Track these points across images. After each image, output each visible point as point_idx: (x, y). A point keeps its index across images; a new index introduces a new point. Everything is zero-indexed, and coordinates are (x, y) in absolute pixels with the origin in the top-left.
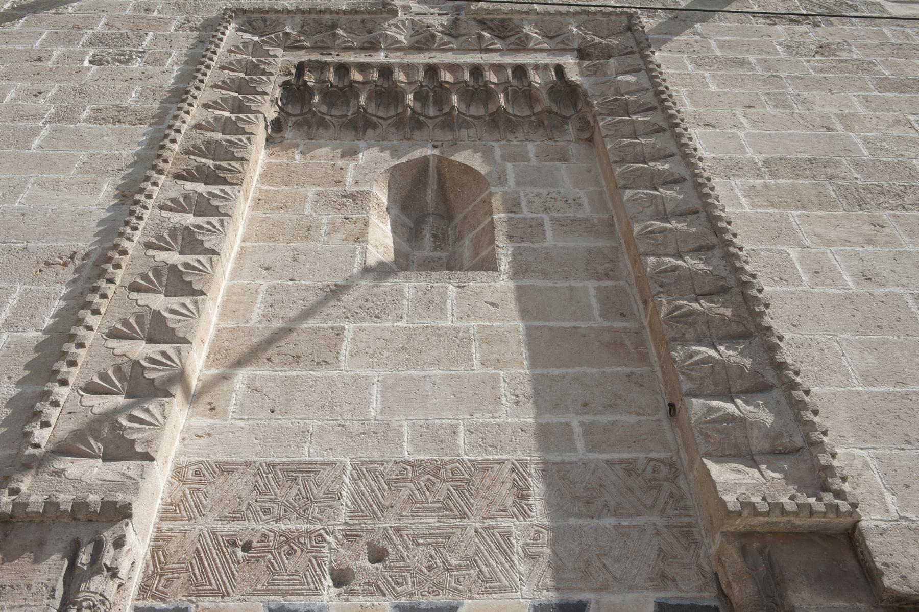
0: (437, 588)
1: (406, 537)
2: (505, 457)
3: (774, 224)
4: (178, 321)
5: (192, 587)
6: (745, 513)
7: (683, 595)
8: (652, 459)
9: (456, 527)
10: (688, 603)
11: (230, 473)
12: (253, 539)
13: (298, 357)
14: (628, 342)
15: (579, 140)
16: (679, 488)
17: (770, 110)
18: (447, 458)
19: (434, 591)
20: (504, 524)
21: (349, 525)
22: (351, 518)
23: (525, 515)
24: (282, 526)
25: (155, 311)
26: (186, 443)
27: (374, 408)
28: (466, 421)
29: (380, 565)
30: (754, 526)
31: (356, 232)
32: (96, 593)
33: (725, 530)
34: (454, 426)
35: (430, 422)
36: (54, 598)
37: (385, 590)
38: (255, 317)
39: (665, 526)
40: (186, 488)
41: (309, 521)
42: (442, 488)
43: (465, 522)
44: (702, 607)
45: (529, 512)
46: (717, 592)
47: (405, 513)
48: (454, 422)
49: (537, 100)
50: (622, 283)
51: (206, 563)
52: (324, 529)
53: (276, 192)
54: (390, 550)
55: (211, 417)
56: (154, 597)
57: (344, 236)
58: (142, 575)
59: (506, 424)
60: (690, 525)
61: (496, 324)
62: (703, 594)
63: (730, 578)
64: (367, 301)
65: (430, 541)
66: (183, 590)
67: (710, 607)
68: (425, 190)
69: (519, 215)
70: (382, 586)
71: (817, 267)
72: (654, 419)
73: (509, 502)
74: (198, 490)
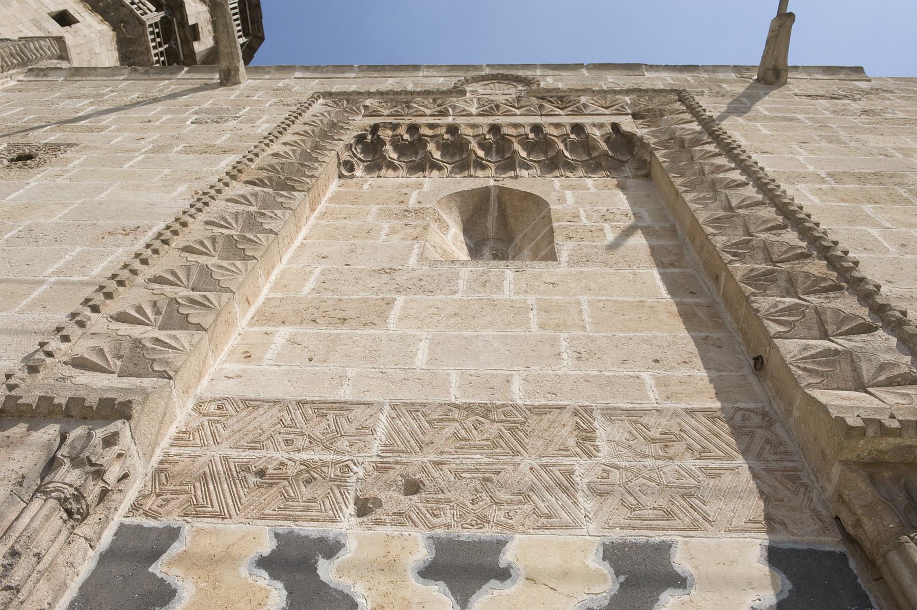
0: (483, 520)
2: (566, 403)
3: (848, 213)
4: (224, 275)
5: (191, 508)
6: (870, 432)
8: (740, 409)
9: (507, 463)
10: (804, 547)
11: (255, 408)
12: (269, 466)
14: (700, 314)
15: (636, 177)
16: (776, 435)
17: (824, 144)
18: (499, 403)
21: (382, 457)
22: (383, 451)
23: (590, 455)
24: (304, 456)
25: (202, 265)
26: (213, 382)
28: (521, 372)
29: (415, 497)
31: (415, 233)
32: (71, 486)
33: (844, 458)
34: (507, 376)
35: (480, 372)
37: (417, 520)
39: (765, 470)
40: (205, 420)
42: (492, 429)
43: (517, 459)
44: (824, 552)
45: (595, 452)
46: (840, 537)
47: (447, 449)
48: (508, 372)
51: (211, 487)
52: (352, 460)
53: (340, 209)
54: (427, 482)
55: (245, 363)
56: (146, 514)
57: (403, 236)
60: (794, 469)
61: (555, 298)
62: (822, 538)
63: (859, 512)
64: (421, 280)
66: (179, 510)
68: (486, 217)
69: (579, 224)
71: (903, 242)
72: (738, 374)
73: (571, 442)
74: (218, 421)
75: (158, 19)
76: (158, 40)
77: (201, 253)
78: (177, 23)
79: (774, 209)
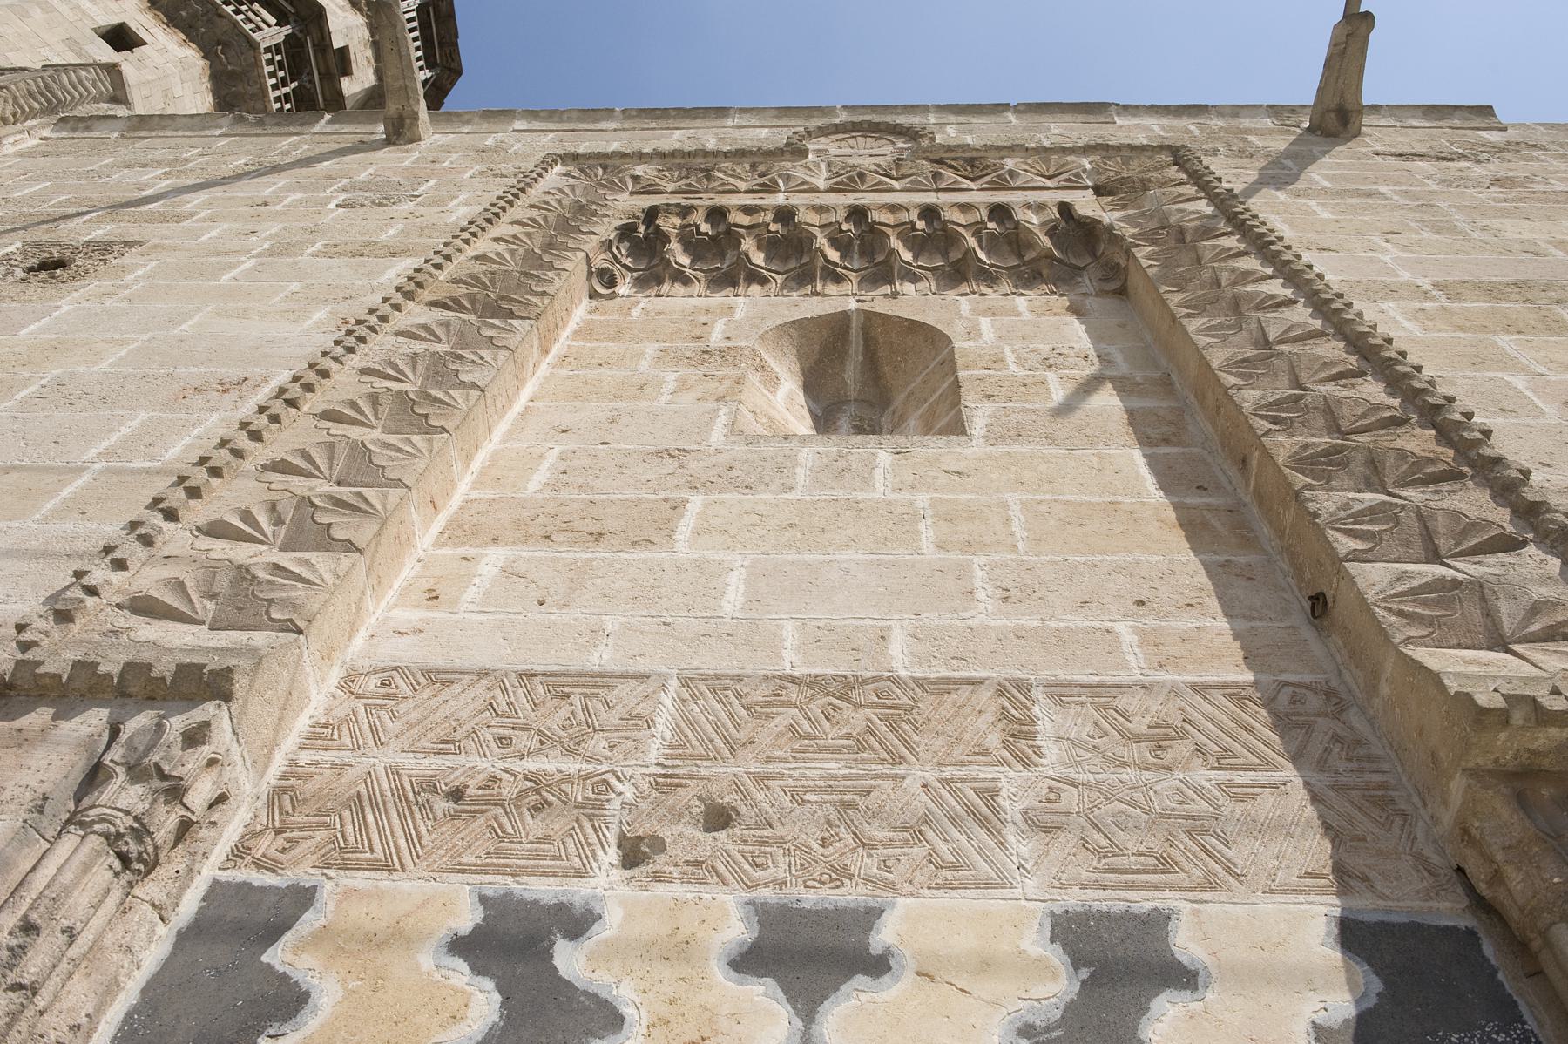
0: (841, 874)
1: (778, 790)
2: (983, 674)
5: (335, 854)
6: (1517, 718)
7: (1390, 903)
8: (1286, 684)
9: (882, 777)
10: (1404, 919)
11: (446, 684)
12: (470, 783)
13: (601, 534)
15: (1101, 293)
16: (1351, 728)
19: (832, 881)
20: (983, 776)
22: (667, 757)
24: (531, 765)
25: (355, 442)
26: (374, 641)
27: (733, 599)
28: (906, 623)
30: (1535, 753)
32: (127, 813)
33: (1471, 765)
34: (881, 629)
36: (41, 812)
38: (532, 487)
39: (1332, 787)
40: (360, 705)
41: (588, 759)
42: (856, 719)
43: (899, 770)
47: (778, 753)
48: (883, 623)
49: (1031, 245)
50: (1196, 450)
51: (370, 818)
52: (613, 772)
54: (743, 809)
56: (257, 865)
58: (241, 830)
59: (985, 627)
60: (1383, 786)
61: (962, 497)
62: (1434, 904)
63: (1499, 857)
65: (828, 797)
67: (1455, 929)
68: (843, 363)
69: (1005, 372)
70: (721, 868)
73: (994, 740)
74: (382, 707)
75: (280, 38)
76: (281, 74)
77: (354, 422)
78: (314, 45)
79: (1342, 344)
